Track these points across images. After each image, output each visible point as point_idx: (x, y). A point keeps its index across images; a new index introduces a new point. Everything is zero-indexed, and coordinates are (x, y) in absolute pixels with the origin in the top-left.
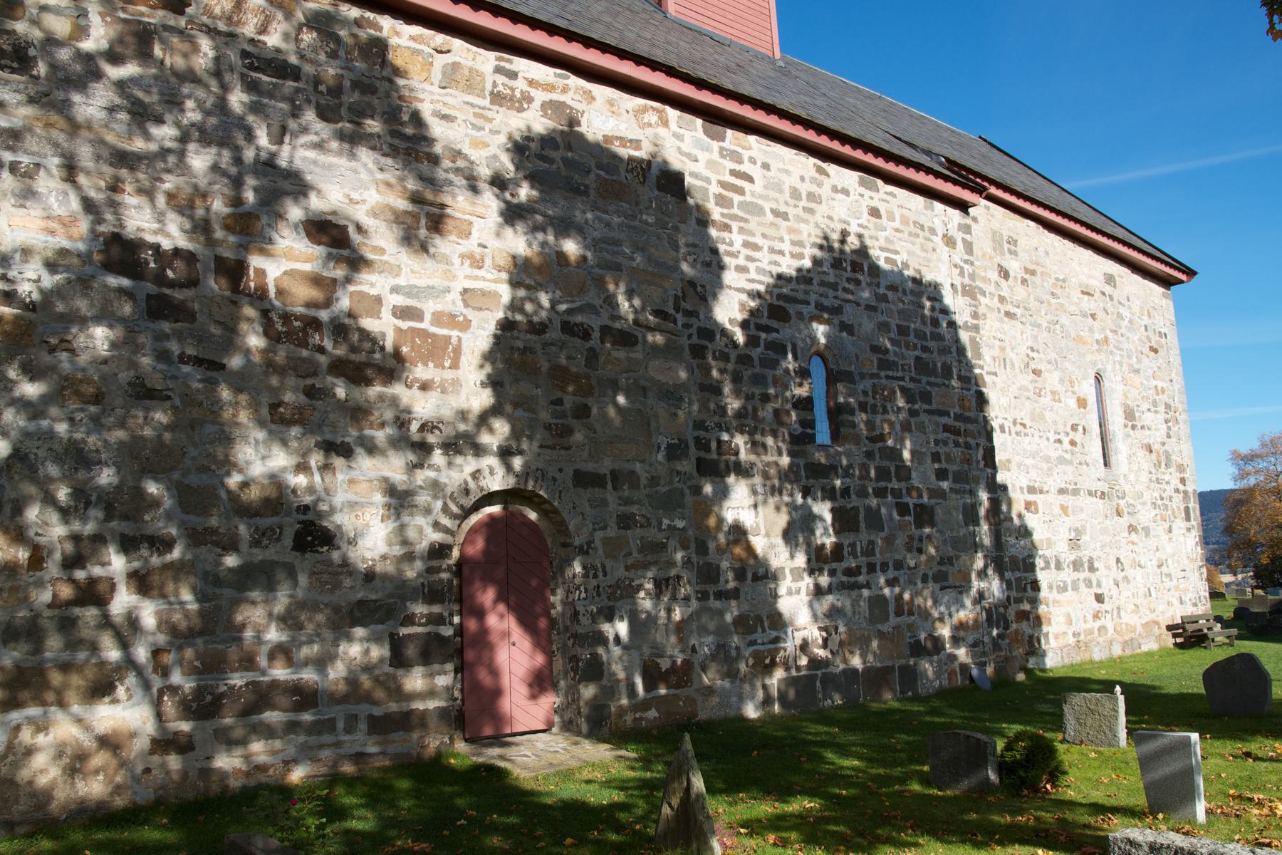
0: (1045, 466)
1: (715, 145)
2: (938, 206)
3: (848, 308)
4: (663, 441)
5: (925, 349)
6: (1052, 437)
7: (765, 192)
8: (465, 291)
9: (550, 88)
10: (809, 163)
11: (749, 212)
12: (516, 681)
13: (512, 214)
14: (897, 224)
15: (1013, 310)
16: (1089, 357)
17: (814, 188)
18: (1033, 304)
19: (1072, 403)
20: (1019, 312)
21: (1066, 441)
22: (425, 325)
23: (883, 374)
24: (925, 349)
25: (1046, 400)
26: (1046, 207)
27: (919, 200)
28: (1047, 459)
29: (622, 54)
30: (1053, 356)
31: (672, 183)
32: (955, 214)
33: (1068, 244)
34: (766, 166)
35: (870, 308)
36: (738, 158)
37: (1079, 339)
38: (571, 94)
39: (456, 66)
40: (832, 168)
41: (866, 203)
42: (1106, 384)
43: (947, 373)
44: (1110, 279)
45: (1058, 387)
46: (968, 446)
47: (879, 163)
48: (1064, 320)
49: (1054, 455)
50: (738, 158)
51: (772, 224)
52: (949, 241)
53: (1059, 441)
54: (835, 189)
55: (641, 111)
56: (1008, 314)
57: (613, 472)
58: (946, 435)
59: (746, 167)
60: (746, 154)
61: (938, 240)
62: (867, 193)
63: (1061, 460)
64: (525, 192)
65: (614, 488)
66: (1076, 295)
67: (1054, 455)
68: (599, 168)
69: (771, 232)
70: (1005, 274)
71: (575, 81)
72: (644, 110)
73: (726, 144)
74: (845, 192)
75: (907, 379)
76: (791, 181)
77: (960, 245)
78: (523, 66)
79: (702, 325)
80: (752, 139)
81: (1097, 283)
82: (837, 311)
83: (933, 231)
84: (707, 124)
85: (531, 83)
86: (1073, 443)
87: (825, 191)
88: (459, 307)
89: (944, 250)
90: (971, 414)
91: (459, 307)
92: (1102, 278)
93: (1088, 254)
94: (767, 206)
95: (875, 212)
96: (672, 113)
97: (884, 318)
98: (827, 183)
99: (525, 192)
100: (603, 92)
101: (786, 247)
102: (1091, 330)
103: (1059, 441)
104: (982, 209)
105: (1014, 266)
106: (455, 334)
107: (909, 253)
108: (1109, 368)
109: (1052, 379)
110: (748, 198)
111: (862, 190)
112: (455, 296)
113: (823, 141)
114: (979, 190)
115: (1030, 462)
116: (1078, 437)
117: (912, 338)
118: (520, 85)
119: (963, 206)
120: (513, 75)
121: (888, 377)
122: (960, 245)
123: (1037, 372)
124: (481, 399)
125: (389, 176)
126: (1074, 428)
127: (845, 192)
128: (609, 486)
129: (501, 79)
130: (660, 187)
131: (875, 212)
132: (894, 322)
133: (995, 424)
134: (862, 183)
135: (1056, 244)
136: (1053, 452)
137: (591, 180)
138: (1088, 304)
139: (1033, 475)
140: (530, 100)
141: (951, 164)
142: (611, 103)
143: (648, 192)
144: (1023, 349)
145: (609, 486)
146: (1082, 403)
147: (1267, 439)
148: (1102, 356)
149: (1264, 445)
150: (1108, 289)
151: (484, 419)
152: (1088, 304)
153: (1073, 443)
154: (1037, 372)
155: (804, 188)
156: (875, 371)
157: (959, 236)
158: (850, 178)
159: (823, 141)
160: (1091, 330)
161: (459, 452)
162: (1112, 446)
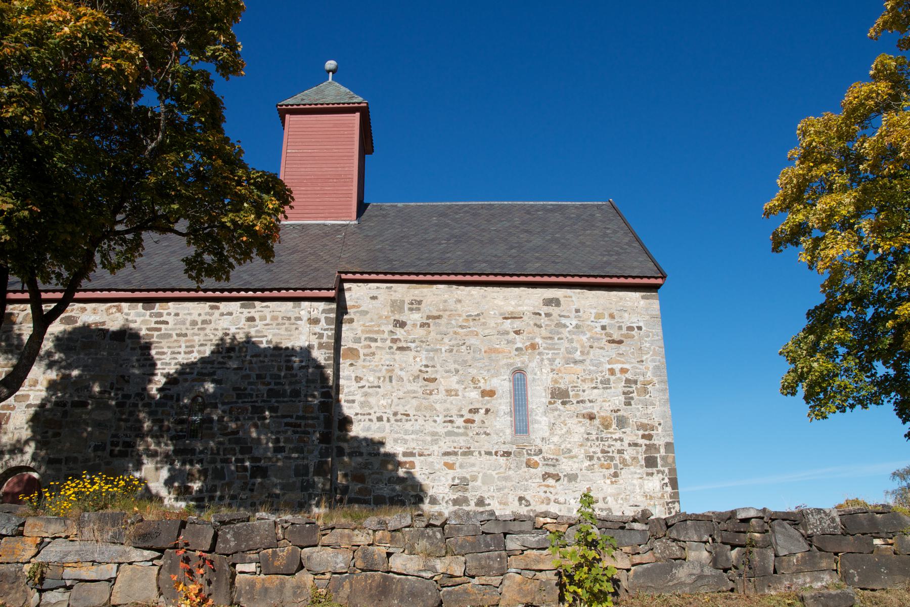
7: (174, 327)
11: (162, 339)
12: (540, 388)
23: (240, 401)
38: (75, 311)
44: (548, 302)
51: (176, 341)
57: (66, 458)
58: (286, 428)
60: (165, 312)
65: (66, 464)
68: (82, 338)
72: (111, 307)
75: (259, 401)
79: (125, 393)
82: (211, 374)
84: (146, 305)
99: (57, 357)
106: (8, 412)
121: (243, 402)
124: (26, 433)
128: (63, 463)
135: (473, 292)
145: (63, 463)
151: (27, 442)
156: (234, 400)
161: (15, 454)
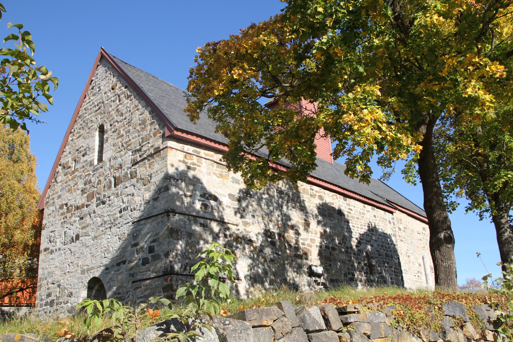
0: (412, 282)
1: (345, 202)
2: (387, 213)
3: (372, 241)
4: (343, 272)
5: (387, 251)
6: (414, 274)
8: (311, 239)
9: (319, 192)
10: (362, 205)
13: (319, 222)
14: (379, 219)
15: (402, 239)
16: (421, 252)
17: (363, 211)
18: (407, 237)
19: (417, 265)
20: (403, 239)
21: (417, 275)
22: (306, 246)
24: (387, 251)
25: (411, 264)
26: (408, 210)
27: (383, 212)
28: (413, 281)
29: (320, 180)
30: (412, 252)
31: (340, 213)
32: (390, 215)
33: (413, 219)
34: (354, 207)
35: (376, 240)
36: (349, 205)
37: (418, 247)
39: (304, 189)
40: (366, 206)
41: (373, 214)
42: (425, 259)
43: (392, 257)
45: (414, 261)
46: (397, 276)
47: (376, 204)
48: (414, 241)
49: (414, 279)
50: (349, 205)
52: (390, 222)
53: (415, 276)
54: (367, 211)
55: (333, 196)
56: (401, 240)
59: (351, 207)
60: (351, 204)
61: (387, 222)
62: (373, 211)
63: (416, 281)
64: (320, 218)
66: (416, 234)
67: (414, 279)
69: (357, 223)
70: (400, 229)
71: (323, 190)
73: (347, 202)
74: (369, 211)
76: (359, 210)
77: (392, 223)
78: (314, 187)
80: (352, 200)
81: (421, 230)
83: (386, 220)
85: (316, 191)
86: (418, 276)
87: (365, 212)
88: (310, 243)
89: (389, 224)
90: (397, 268)
91: (310, 243)
92: (422, 229)
93: (418, 222)
94: (355, 216)
95: (375, 216)
96: (338, 195)
97: (378, 243)
98: (366, 209)
100: (327, 192)
101: (359, 226)
102: (420, 244)
103: (415, 276)
104: (397, 214)
105: (402, 227)
107: (382, 226)
108: (426, 255)
109: (412, 258)
110: (352, 215)
111: (372, 211)
112: (309, 240)
113: (365, 200)
114: (396, 209)
115: (409, 281)
116: (419, 274)
117: (384, 248)
118: (314, 192)
119: (392, 213)
120: (313, 190)
122: (392, 223)
123: (409, 256)
125: (300, 216)
126: (418, 272)
127: (369, 211)
129: (311, 191)
130: (338, 214)
131: (375, 216)
132: (380, 244)
133: (403, 271)
134: (372, 209)
136: (414, 279)
137: (327, 213)
138: (419, 236)
139: (410, 285)
140: (316, 195)
141: (388, 201)
142: (328, 194)
143: (336, 215)
144: (405, 250)
146: (420, 265)
147: (469, 281)
148: (424, 251)
149: (468, 283)
150: (424, 232)
152: (419, 236)
153: (418, 276)
154: (409, 256)
155: (362, 211)
157: (392, 221)
158: (369, 208)
159: (365, 200)
160: (420, 244)
162: (428, 277)
